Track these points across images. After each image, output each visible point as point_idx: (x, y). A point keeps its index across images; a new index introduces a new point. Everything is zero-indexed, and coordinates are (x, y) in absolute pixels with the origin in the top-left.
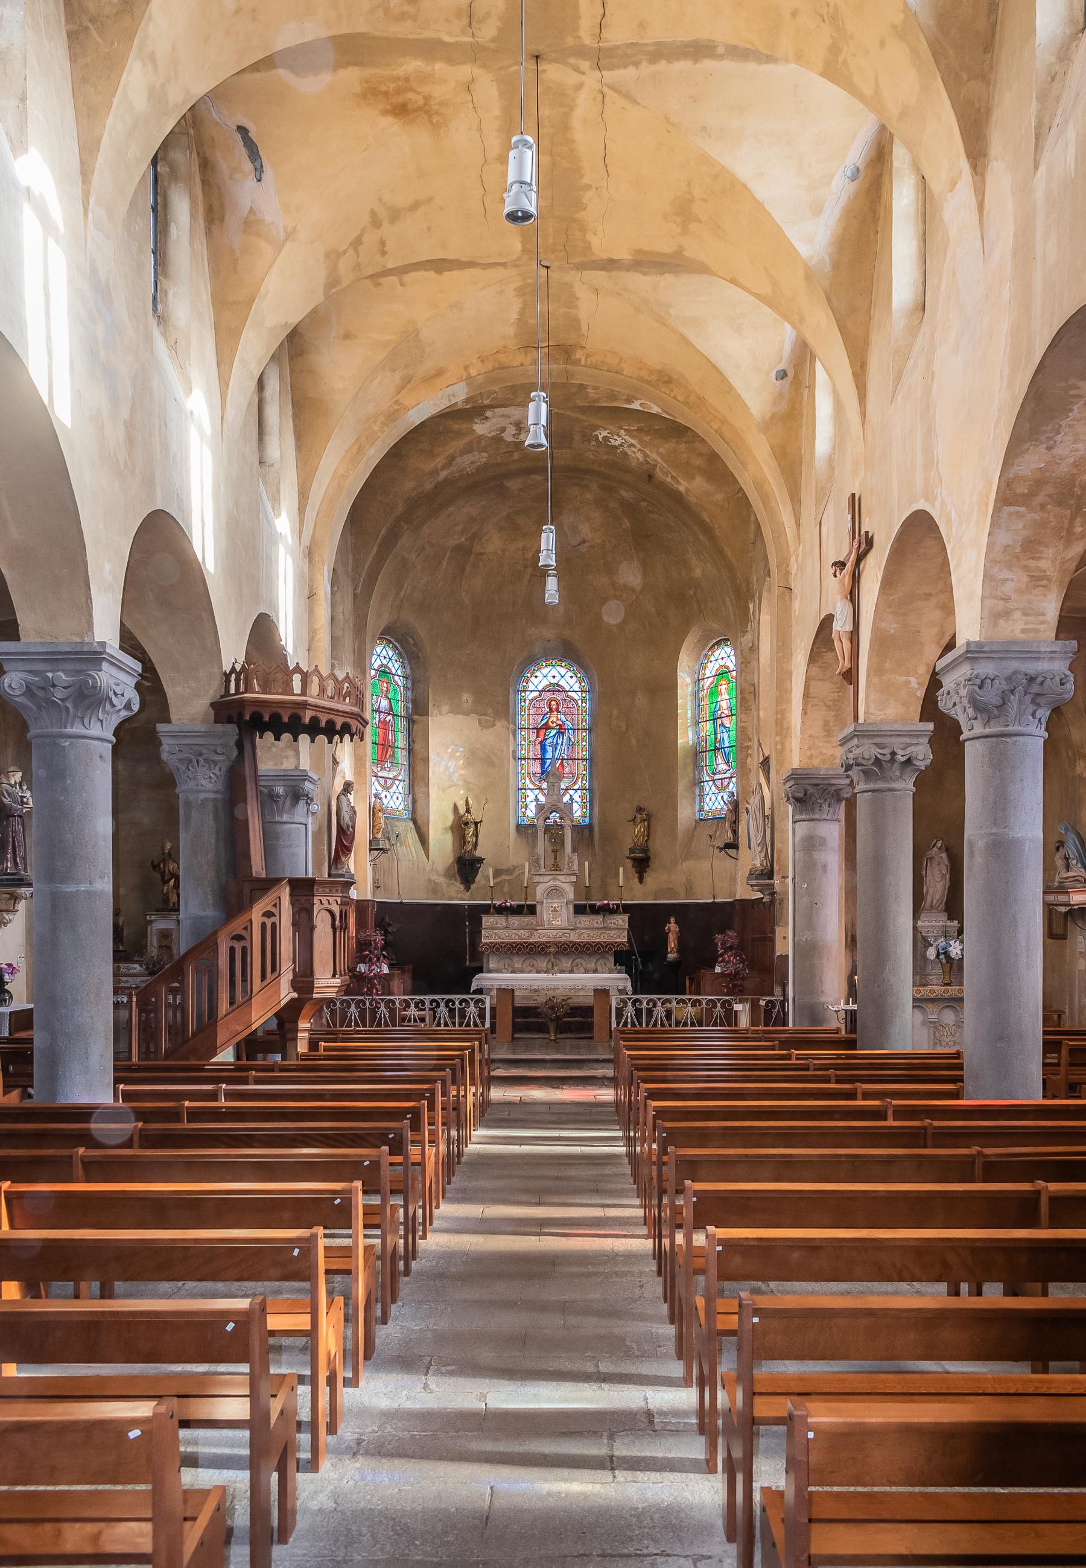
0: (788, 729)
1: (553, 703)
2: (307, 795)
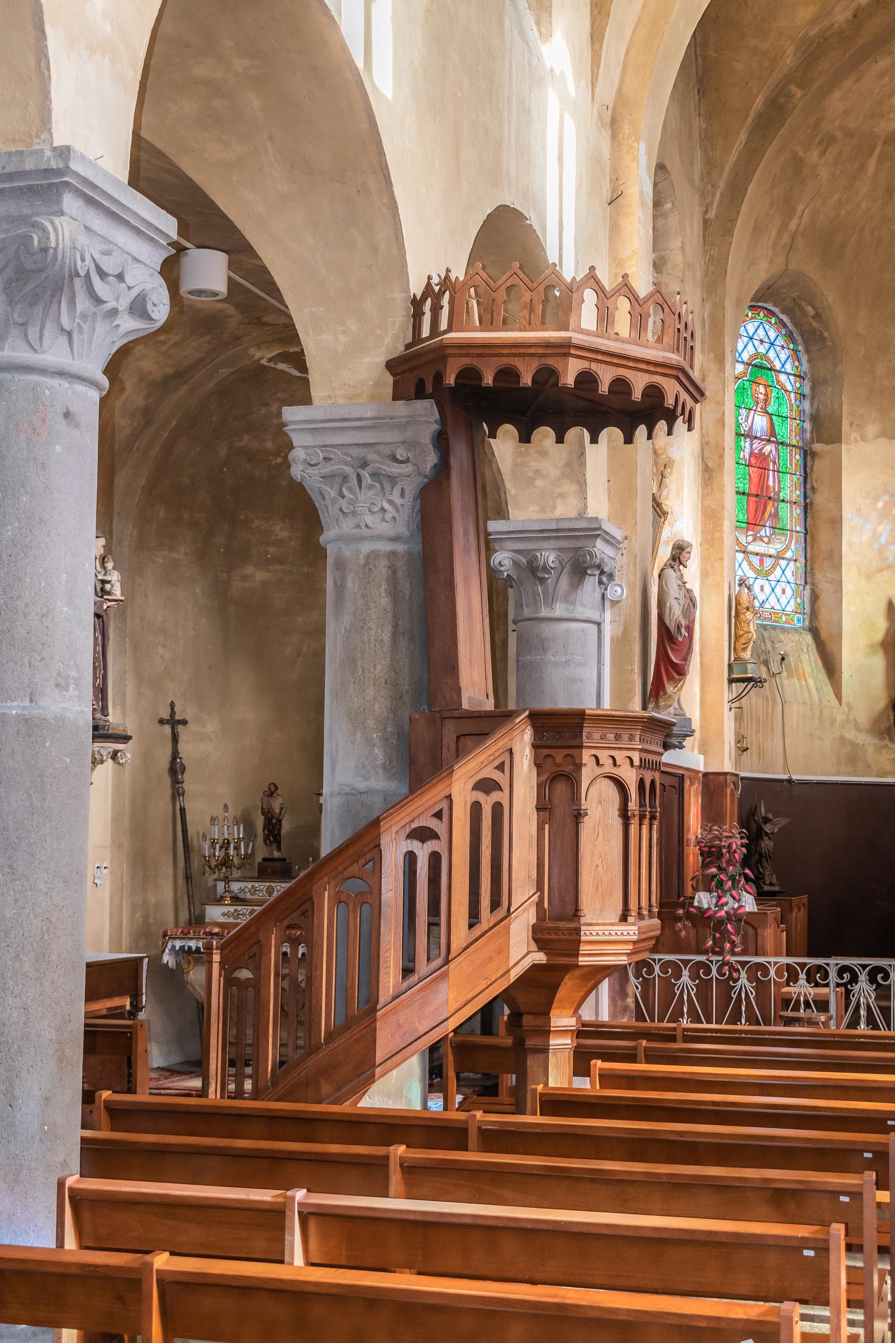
2: (599, 567)
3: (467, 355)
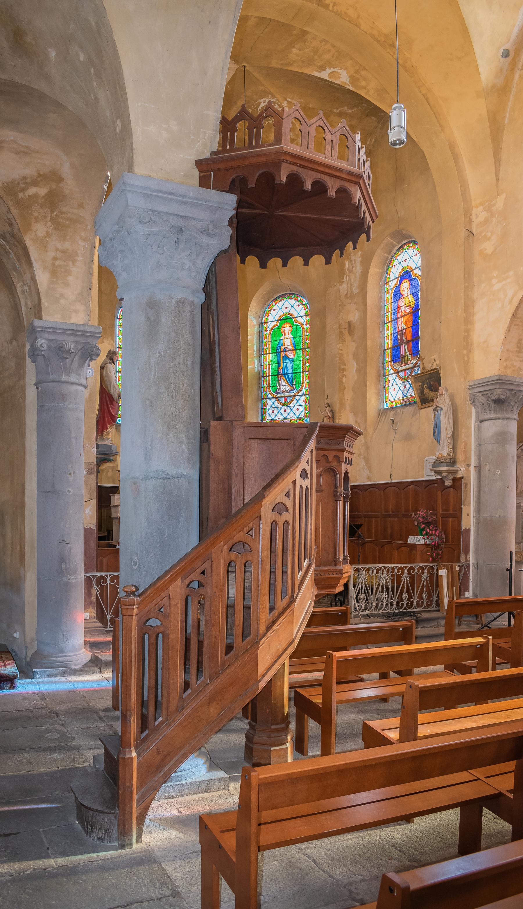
0: (471, 345)
3: (295, 164)
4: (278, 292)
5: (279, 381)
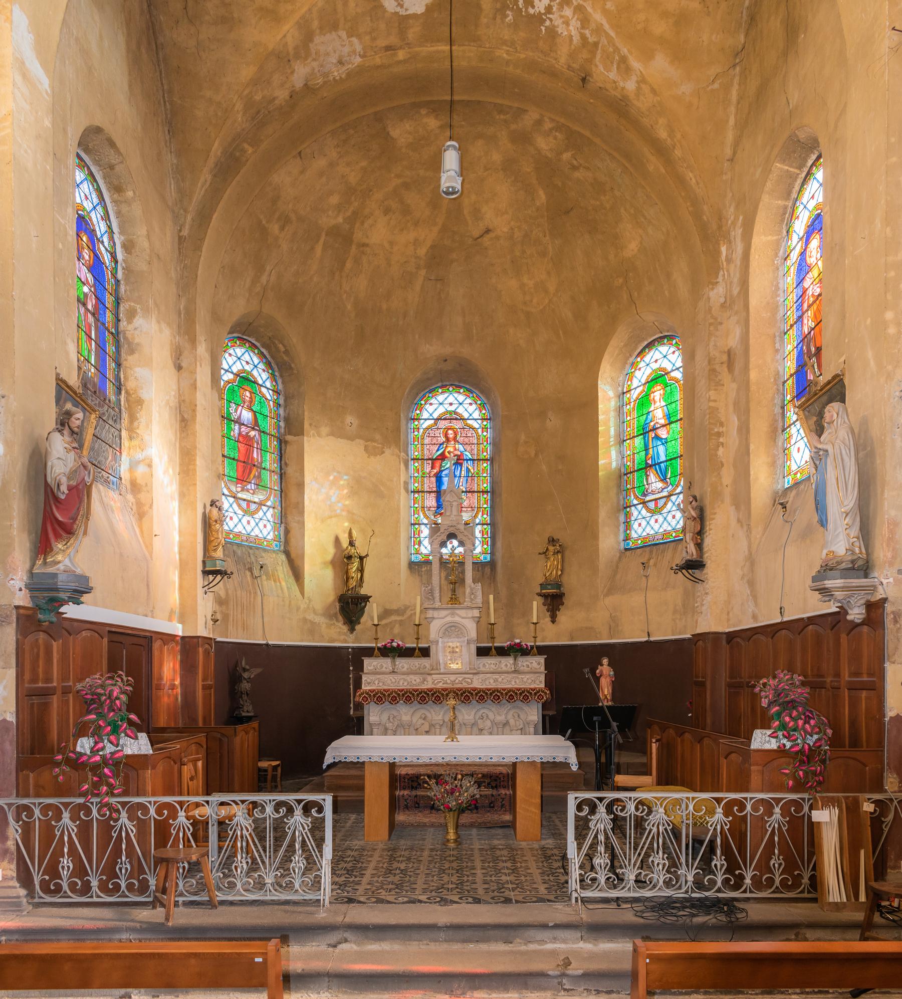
1: (450, 432)
4: (643, 340)
5: (647, 476)
